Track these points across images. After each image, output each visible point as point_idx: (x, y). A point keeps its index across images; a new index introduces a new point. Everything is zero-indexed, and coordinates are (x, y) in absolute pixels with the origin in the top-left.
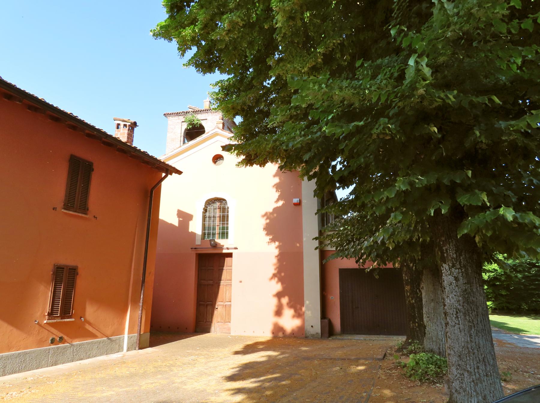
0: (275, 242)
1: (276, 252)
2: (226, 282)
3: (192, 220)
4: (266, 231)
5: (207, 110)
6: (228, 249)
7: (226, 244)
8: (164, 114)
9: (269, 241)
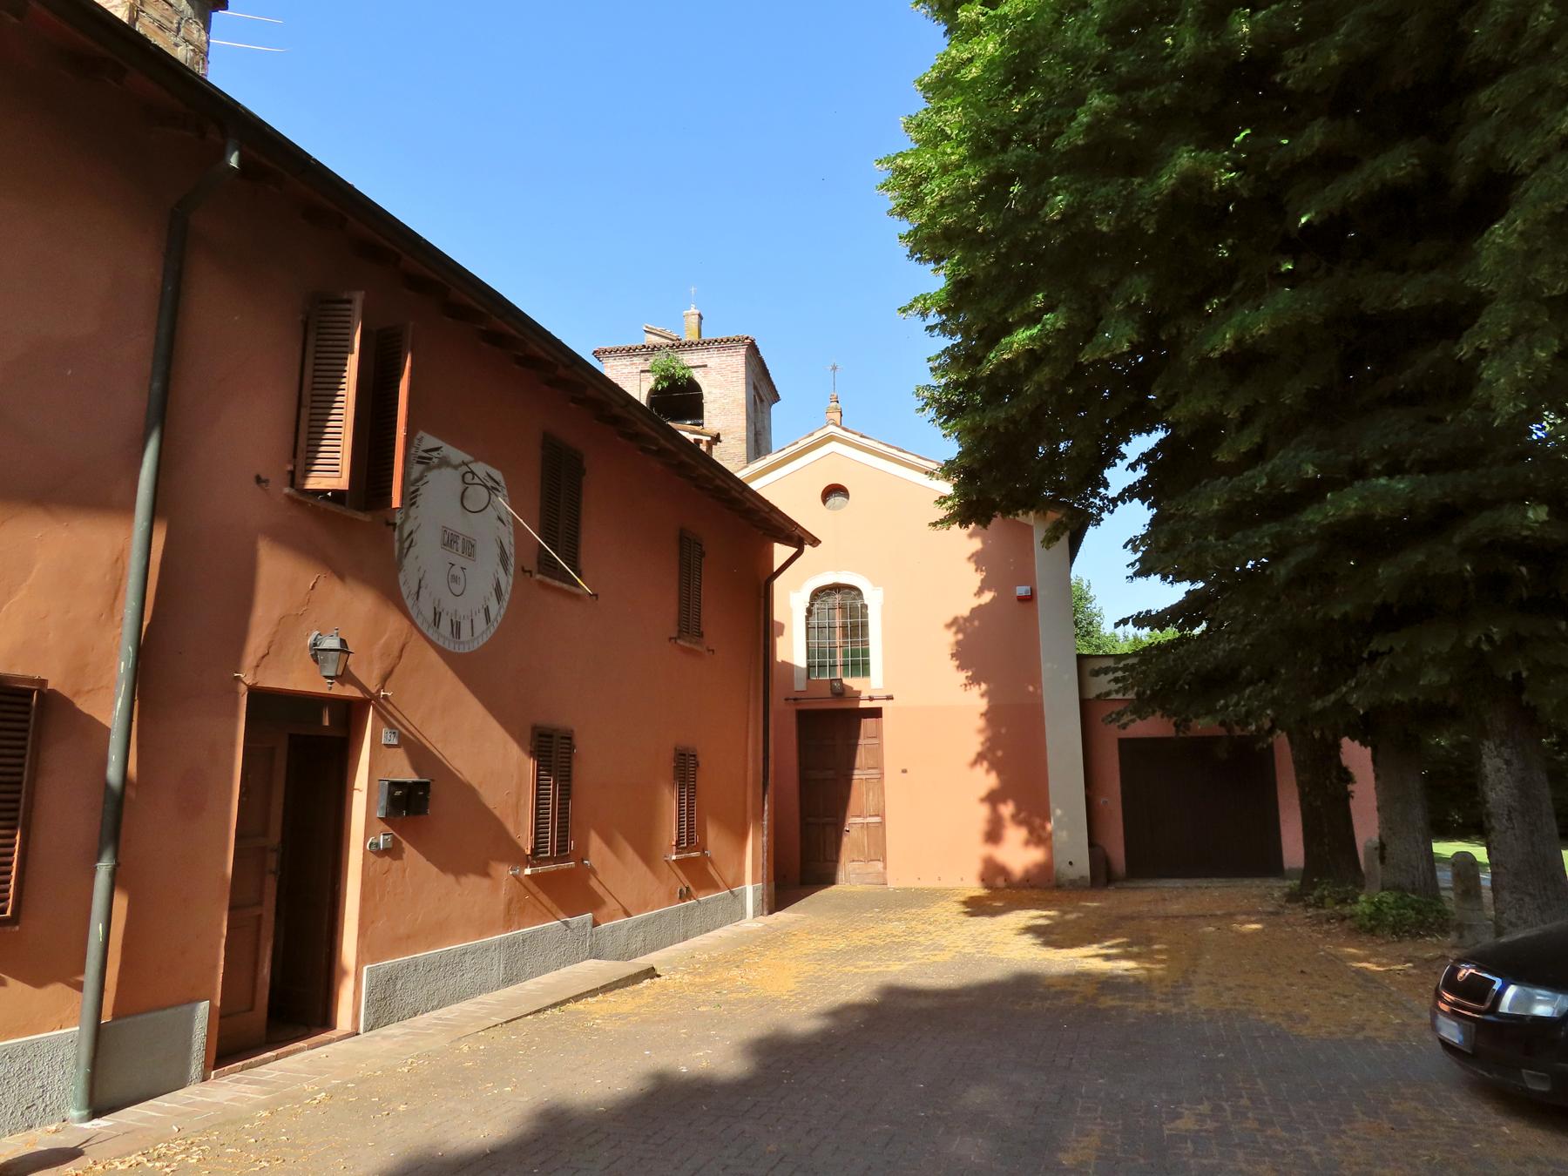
0: (980, 685)
1: (983, 704)
2: (865, 772)
3: (782, 634)
4: (957, 660)
5: (708, 344)
6: (871, 699)
7: (869, 687)
8: (595, 352)
9: (965, 681)
